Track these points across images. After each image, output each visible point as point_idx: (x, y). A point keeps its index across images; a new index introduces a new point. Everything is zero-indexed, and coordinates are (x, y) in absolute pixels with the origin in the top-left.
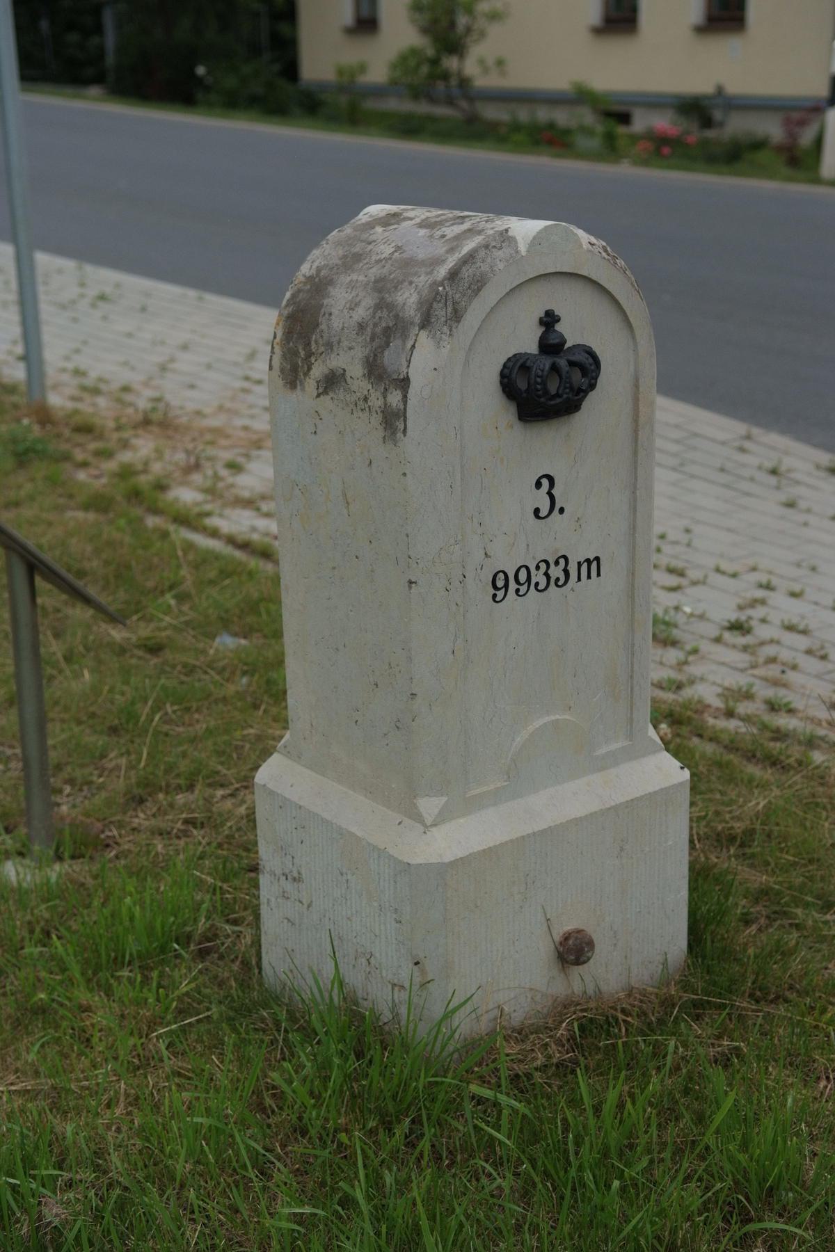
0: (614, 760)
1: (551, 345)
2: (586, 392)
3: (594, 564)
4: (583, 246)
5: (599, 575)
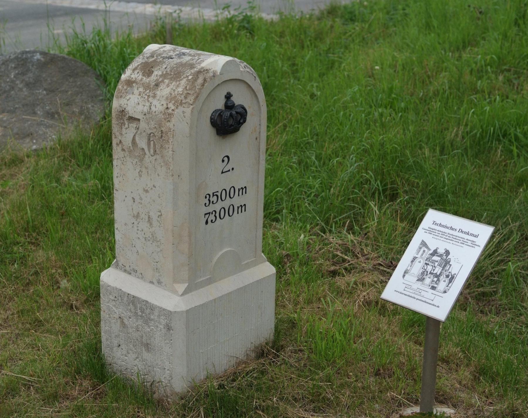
0: (248, 266)
1: (229, 105)
2: (242, 124)
3: (244, 189)
4: (243, 69)
5: (245, 211)
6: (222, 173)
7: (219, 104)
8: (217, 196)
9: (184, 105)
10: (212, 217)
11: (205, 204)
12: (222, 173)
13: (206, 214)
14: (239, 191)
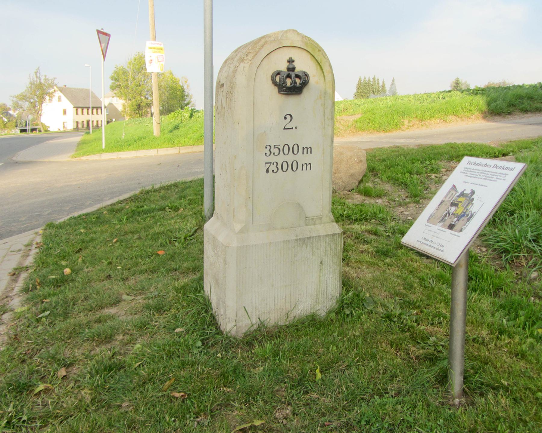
3: (309, 150)
6: (285, 129)
7: (283, 67)
8: (279, 149)
9: (245, 61)
10: (273, 167)
11: (266, 154)
12: (285, 129)
13: (266, 163)
14: (303, 149)
